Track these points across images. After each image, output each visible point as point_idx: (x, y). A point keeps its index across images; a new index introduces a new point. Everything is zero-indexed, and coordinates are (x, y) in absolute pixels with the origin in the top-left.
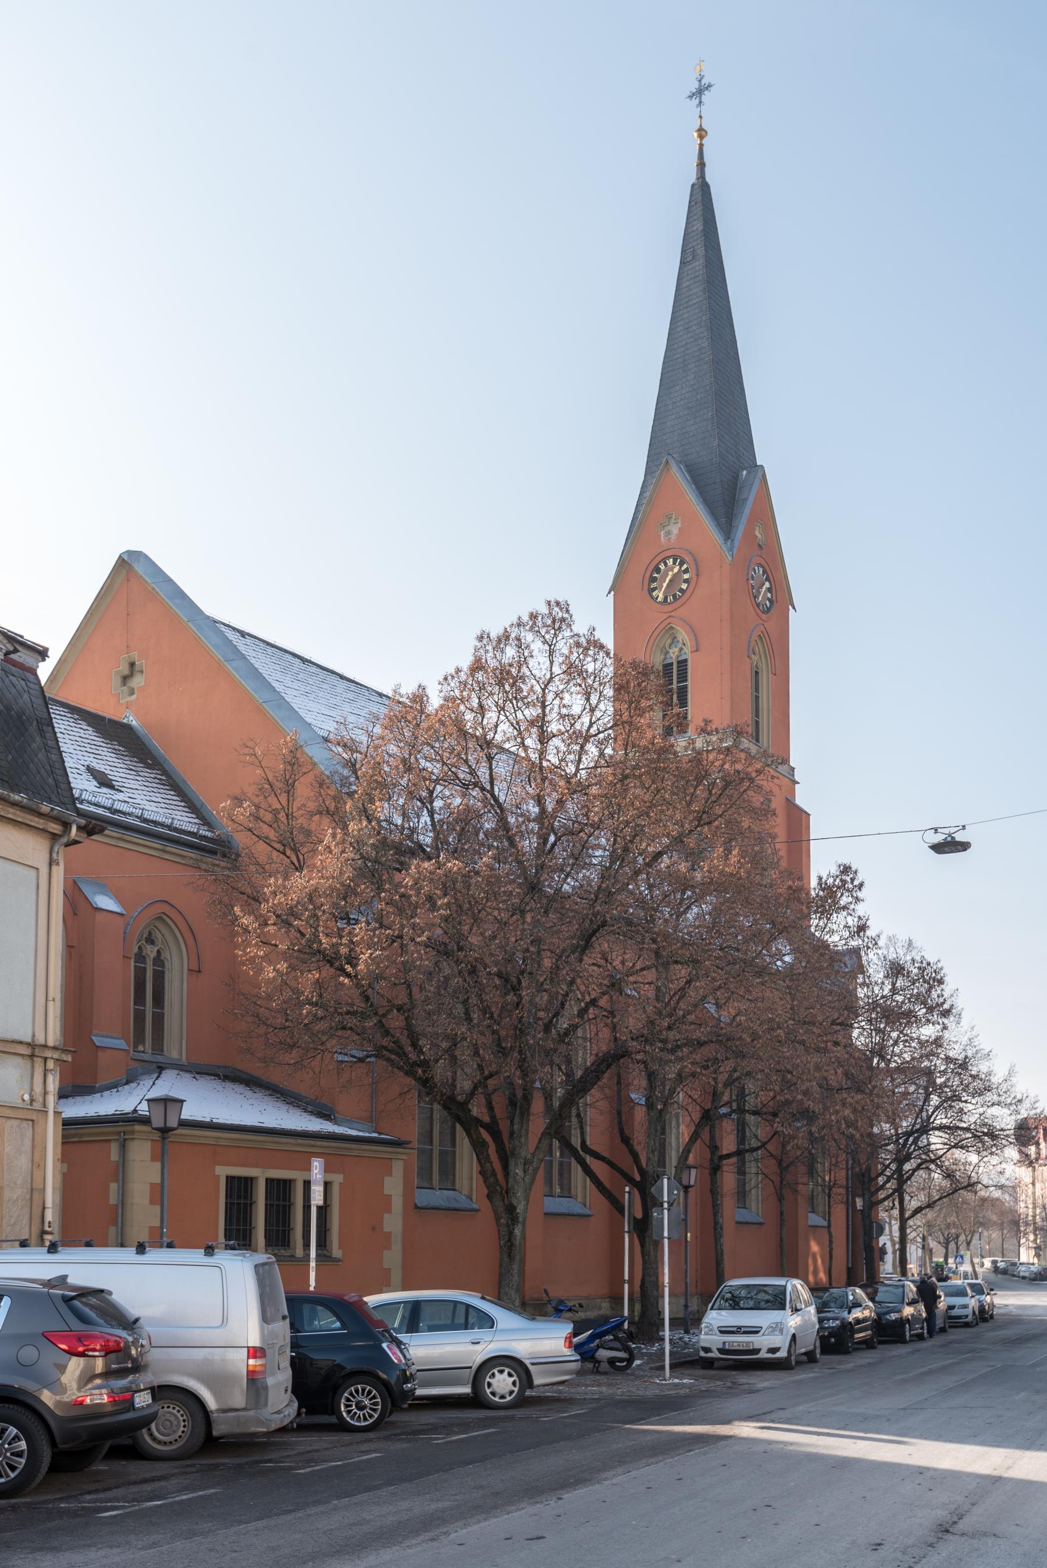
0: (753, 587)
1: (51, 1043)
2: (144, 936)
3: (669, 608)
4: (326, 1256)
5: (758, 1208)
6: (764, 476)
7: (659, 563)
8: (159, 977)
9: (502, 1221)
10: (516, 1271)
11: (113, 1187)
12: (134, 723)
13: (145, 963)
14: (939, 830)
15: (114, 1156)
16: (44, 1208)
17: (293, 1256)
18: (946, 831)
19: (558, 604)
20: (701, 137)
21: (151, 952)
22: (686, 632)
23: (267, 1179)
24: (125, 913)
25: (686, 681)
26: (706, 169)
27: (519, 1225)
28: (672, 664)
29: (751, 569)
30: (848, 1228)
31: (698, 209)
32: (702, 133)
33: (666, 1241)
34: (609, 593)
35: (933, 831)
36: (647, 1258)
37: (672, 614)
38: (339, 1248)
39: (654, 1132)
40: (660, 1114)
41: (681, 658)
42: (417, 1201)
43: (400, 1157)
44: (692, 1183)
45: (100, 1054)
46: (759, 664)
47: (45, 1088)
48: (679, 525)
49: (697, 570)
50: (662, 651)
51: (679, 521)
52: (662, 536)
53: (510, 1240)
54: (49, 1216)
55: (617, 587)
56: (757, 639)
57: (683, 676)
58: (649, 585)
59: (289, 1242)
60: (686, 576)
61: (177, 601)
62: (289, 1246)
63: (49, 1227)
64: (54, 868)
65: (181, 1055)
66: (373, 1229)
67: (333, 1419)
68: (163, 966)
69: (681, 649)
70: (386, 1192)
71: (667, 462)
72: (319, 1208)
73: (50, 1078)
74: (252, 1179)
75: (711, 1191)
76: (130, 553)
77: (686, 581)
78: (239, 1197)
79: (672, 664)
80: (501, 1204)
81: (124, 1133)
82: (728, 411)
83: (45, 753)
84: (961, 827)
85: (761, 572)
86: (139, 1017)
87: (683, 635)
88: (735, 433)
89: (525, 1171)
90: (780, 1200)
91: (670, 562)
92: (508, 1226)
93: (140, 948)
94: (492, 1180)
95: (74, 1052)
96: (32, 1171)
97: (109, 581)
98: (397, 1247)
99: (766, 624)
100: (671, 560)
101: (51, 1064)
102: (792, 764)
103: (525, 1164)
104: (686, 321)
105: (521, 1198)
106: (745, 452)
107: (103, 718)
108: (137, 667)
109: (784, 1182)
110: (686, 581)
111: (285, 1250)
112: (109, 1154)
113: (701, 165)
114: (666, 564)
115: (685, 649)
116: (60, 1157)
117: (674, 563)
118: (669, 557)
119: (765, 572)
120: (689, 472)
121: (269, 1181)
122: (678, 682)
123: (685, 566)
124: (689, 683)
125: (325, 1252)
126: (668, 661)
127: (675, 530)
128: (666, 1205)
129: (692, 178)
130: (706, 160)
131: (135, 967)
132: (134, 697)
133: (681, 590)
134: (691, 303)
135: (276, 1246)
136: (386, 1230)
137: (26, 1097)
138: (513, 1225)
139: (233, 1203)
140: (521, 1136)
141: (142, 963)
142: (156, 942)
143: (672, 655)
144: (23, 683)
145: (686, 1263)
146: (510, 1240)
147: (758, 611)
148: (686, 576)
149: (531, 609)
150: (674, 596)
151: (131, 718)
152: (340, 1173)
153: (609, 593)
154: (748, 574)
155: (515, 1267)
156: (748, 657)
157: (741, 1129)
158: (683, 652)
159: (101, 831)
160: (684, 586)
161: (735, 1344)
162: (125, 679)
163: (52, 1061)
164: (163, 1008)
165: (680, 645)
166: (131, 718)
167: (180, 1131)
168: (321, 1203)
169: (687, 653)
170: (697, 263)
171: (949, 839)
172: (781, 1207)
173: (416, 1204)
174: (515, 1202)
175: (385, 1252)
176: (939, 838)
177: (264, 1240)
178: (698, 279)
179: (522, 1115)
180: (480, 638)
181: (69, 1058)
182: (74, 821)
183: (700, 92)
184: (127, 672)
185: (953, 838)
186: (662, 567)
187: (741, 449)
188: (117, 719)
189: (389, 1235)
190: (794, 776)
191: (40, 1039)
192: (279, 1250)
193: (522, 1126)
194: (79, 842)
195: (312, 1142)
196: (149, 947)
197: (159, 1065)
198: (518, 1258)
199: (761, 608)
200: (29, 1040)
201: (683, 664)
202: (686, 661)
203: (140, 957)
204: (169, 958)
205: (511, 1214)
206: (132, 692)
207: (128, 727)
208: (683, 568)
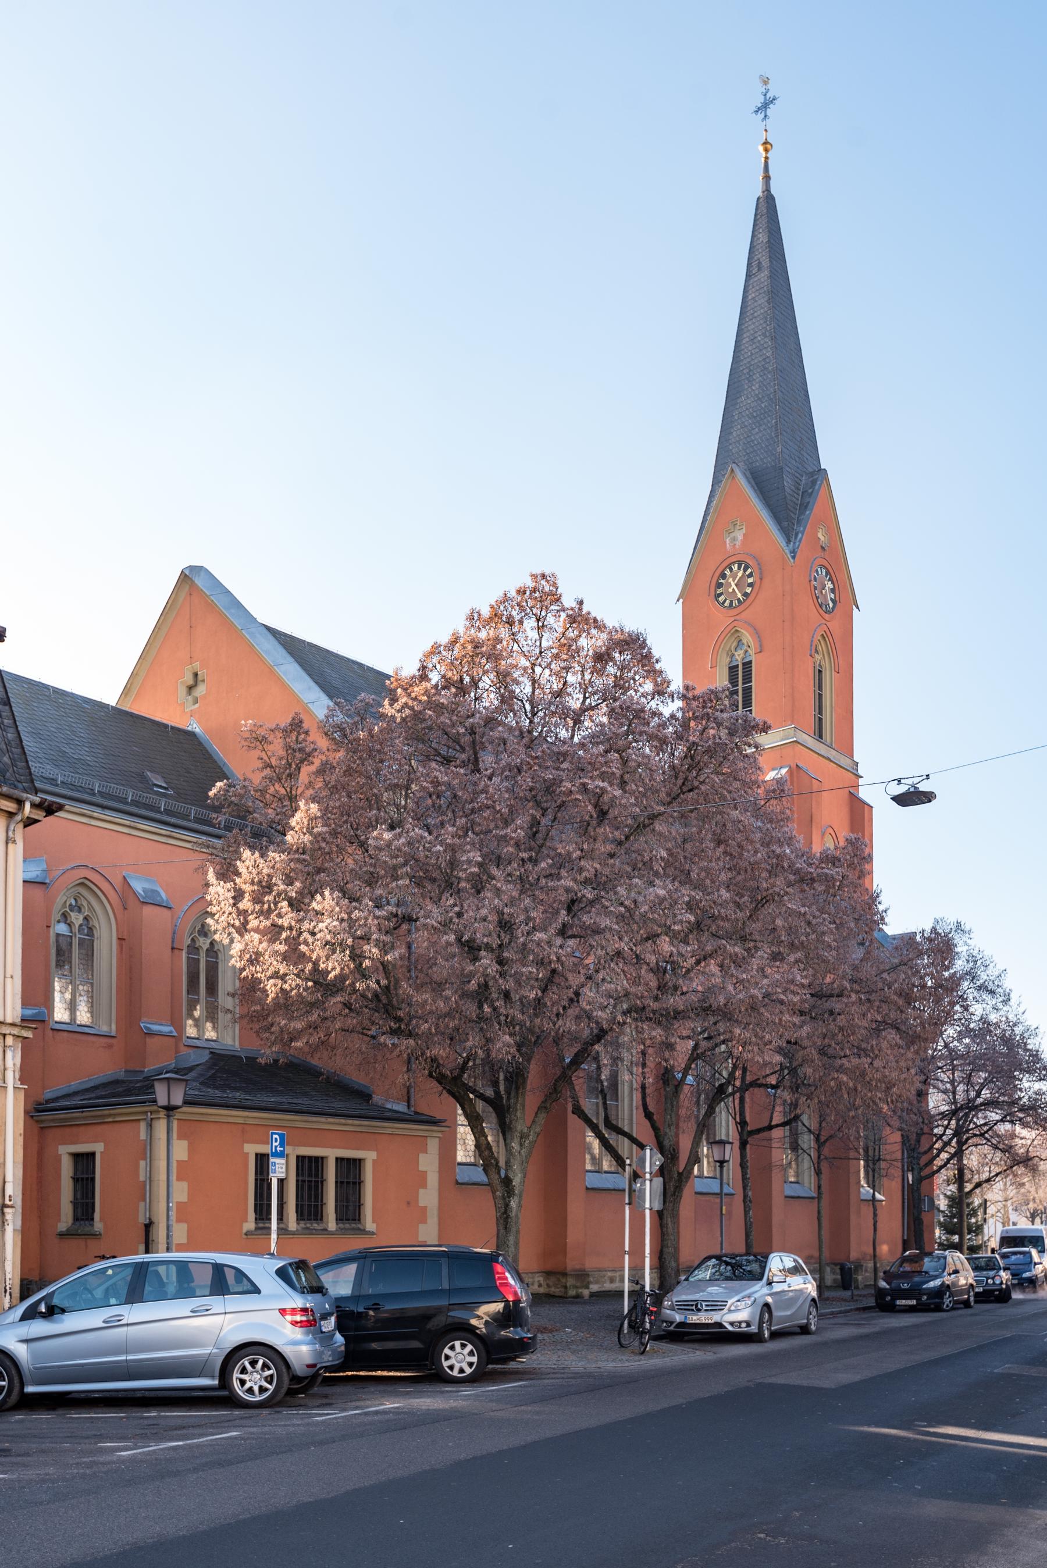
1: (9, 1020)
2: (197, 929)
3: (736, 611)
4: (359, 1229)
5: (810, 1183)
7: (725, 569)
9: (498, 1193)
10: (512, 1242)
11: (142, 1163)
12: (197, 730)
13: (199, 954)
14: (902, 781)
15: (143, 1135)
16: (4, 1182)
17: (326, 1230)
18: (910, 781)
19: (543, 576)
20: (766, 150)
22: (750, 635)
23: (298, 1157)
25: (751, 681)
26: (772, 182)
27: (515, 1197)
28: (737, 666)
29: (813, 570)
30: (903, 1202)
31: (763, 222)
34: (678, 600)
35: (896, 782)
36: (665, 1229)
37: (737, 618)
38: (373, 1222)
39: (670, 1107)
40: (676, 1089)
42: (458, 1178)
43: (435, 1134)
44: (727, 1158)
45: (148, 1040)
46: (823, 663)
47: (4, 1065)
48: (744, 531)
49: (761, 573)
50: (728, 654)
51: (744, 527)
52: (728, 542)
53: (505, 1212)
55: (687, 594)
56: (819, 638)
57: (748, 678)
58: (716, 591)
59: (322, 1216)
60: (750, 580)
61: (233, 611)
62: (321, 1219)
63: (10, 1200)
64: (10, 846)
65: (234, 1041)
66: (408, 1203)
68: (217, 957)
69: (746, 651)
70: (421, 1169)
71: (732, 470)
74: (322, 1158)
75: (741, 1165)
76: (191, 568)
77: (751, 585)
78: (310, 1175)
79: (737, 666)
80: (497, 1177)
81: (151, 1112)
82: (791, 417)
84: (925, 777)
85: (824, 574)
87: (747, 637)
88: (799, 439)
89: (521, 1145)
90: (817, 1174)
91: (735, 567)
92: (504, 1198)
93: (193, 940)
94: (486, 1153)
95: (35, 1028)
98: (433, 1220)
99: (828, 624)
100: (736, 565)
101: (10, 1040)
103: (521, 1138)
104: (752, 332)
105: (517, 1171)
107: (166, 726)
108: (200, 678)
109: (822, 1157)
110: (751, 585)
111: (318, 1224)
112: (139, 1133)
113: (767, 178)
114: (731, 570)
115: (750, 652)
116: (22, 1132)
117: (739, 568)
118: (734, 563)
119: (828, 573)
120: (754, 478)
121: (338, 1160)
122: (744, 683)
123: (749, 571)
124: (753, 684)
125: (359, 1226)
127: (739, 535)
128: (648, 1176)
129: (759, 192)
130: (771, 173)
131: (188, 958)
132: (197, 706)
134: (756, 314)
135: (308, 1220)
136: (421, 1203)
138: (509, 1197)
139: (304, 1181)
140: (516, 1110)
142: (83, 910)
143: (737, 657)
145: (722, 1236)
146: (505, 1212)
147: (821, 611)
148: (750, 580)
149: (519, 584)
151: (195, 726)
153: (678, 600)
154: (810, 575)
155: (512, 1238)
156: (811, 656)
157: (988, 1130)
158: (747, 654)
159: (61, 807)
160: (748, 590)
162: (190, 688)
163: (11, 1037)
165: (745, 648)
166: (195, 726)
167: (185, 1109)
169: (752, 657)
170: (762, 275)
171: (912, 790)
172: (819, 1180)
173: (457, 1181)
174: (511, 1175)
175: (420, 1225)
176: (902, 789)
177: (334, 1215)
178: (762, 291)
179: (517, 1089)
180: (471, 618)
181: (29, 1034)
182: (27, 799)
183: (765, 106)
184: (191, 682)
185: (915, 788)
186: (728, 572)
187: (805, 454)
188: (181, 727)
189: (425, 1208)
192: (312, 1224)
193: (517, 1101)
194: (36, 821)
195: (343, 1121)
196: (201, 939)
198: (514, 1230)
199: (824, 608)
201: (747, 665)
202: (750, 662)
203: (193, 948)
204: (222, 949)
205: (507, 1187)
206: (196, 701)
207: (192, 735)
208: (747, 573)
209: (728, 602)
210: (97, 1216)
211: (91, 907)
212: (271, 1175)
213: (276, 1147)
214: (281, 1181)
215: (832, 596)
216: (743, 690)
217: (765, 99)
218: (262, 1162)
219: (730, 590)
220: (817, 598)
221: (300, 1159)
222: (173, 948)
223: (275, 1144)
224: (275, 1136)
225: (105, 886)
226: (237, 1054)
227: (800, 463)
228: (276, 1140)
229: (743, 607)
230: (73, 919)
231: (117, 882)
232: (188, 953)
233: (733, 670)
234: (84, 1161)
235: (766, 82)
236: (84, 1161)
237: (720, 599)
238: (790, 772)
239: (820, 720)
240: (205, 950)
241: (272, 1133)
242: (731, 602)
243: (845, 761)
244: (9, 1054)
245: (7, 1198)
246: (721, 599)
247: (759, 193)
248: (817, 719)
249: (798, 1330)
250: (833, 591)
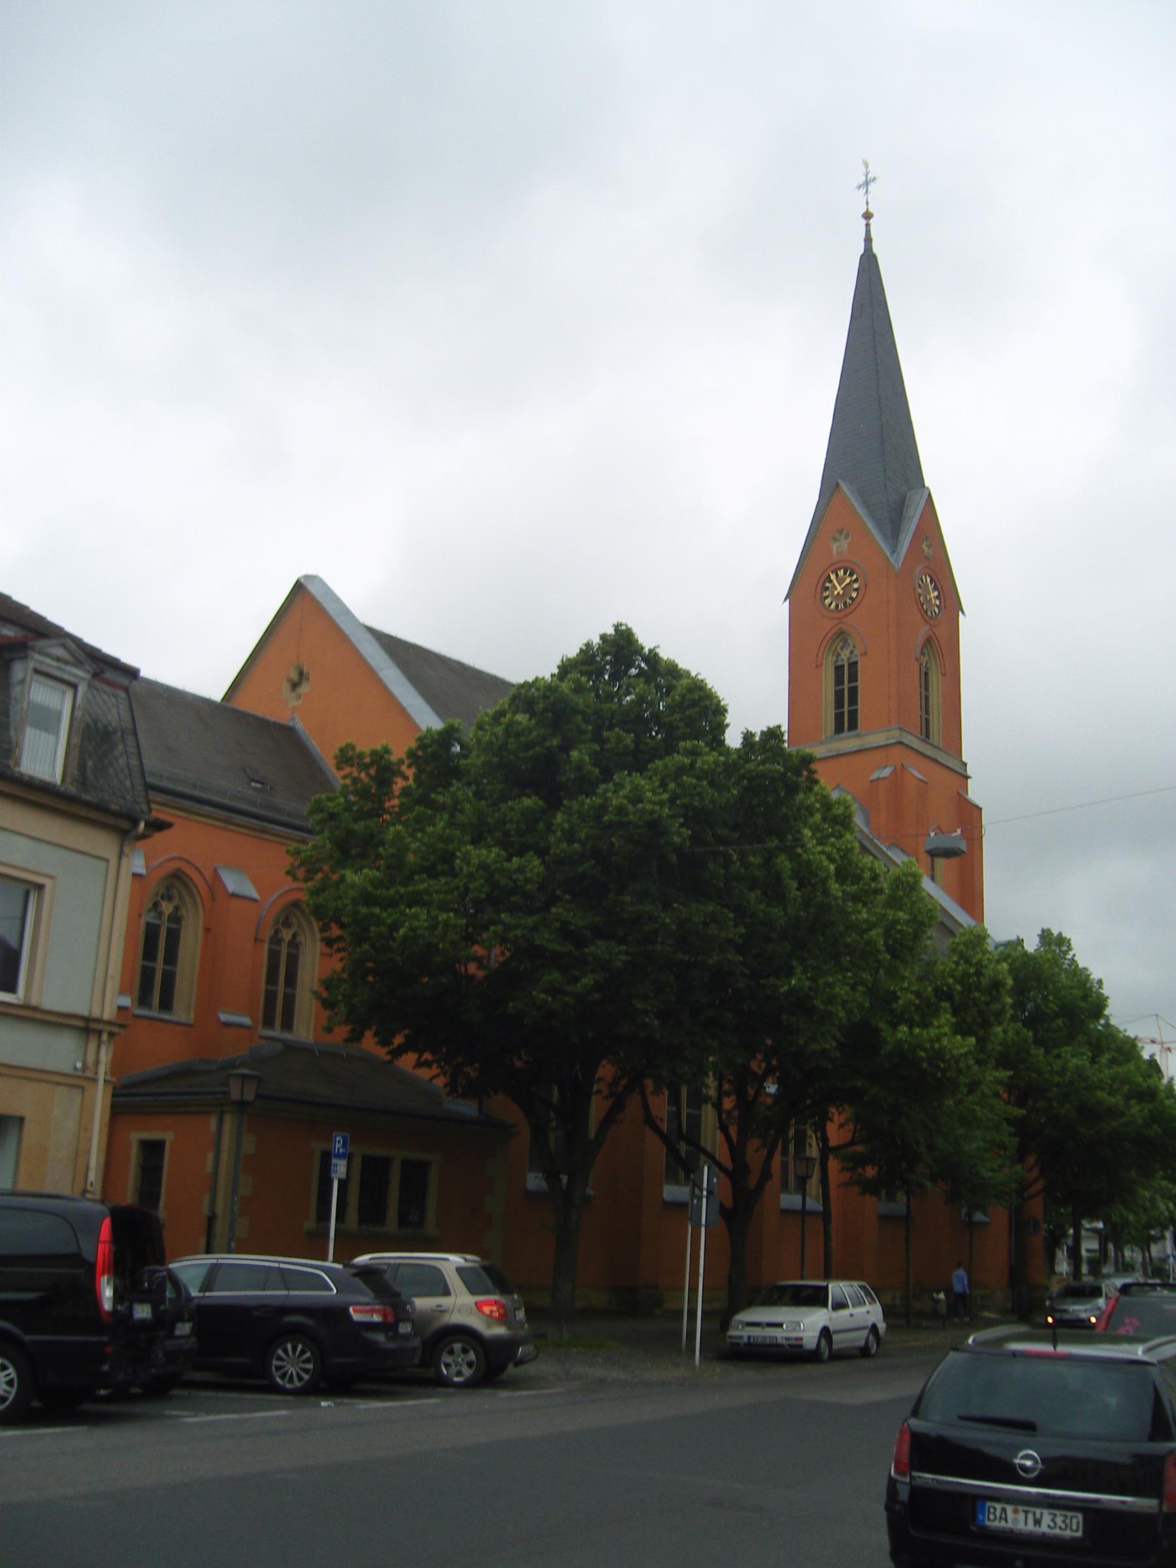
0: (920, 595)
1: (106, 1016)
3: (840, 615)
6: (930, 495)
8: (293, 961)
21: (287, 935)
25: (857, 681)
32: (868, 216)
41: (851, 661)
57: (853, 677)
60: (856, 586)
67: (266, 1382)
73: (103, 1049)
76: (307, 577)
79: (843, 666)
86: (270, 998)
97: (288, 600)
100: (842, 571)
102: (964, 759)
113: (868, 240)
115: (856, 652)
117: (845, 573)
121: (406, 1163)
123: (854, 577)
124: (859, 683)
126: (840, 663)
130: (873, 235)
133: (851, 598)
137: (79, 1065)
148: (856, 586)
150: (845, 604)
152: (779, 1197)
160: (854, 595)
162: (295, 686)
168: (343, 1176)
191: (96, 1013)
200: (86, 1013)
201: (853, 666)
202: (856, 663)
210: (162, 1204)
213: (338, 1149)
214: (342, 1183)
217: (867, 179)
219: (836, 593)
220: (922, 605)
221: (366, 1160)
225: (196, 877)
228: (339, 1142)
229: (849, 610)
233: (839, 669)
235: (866, 165)
236: (152, 1150)
239: (927, 721)
240: (287, 942)
246: (827, 601)
247: (862, 251)
248: (924, 720)
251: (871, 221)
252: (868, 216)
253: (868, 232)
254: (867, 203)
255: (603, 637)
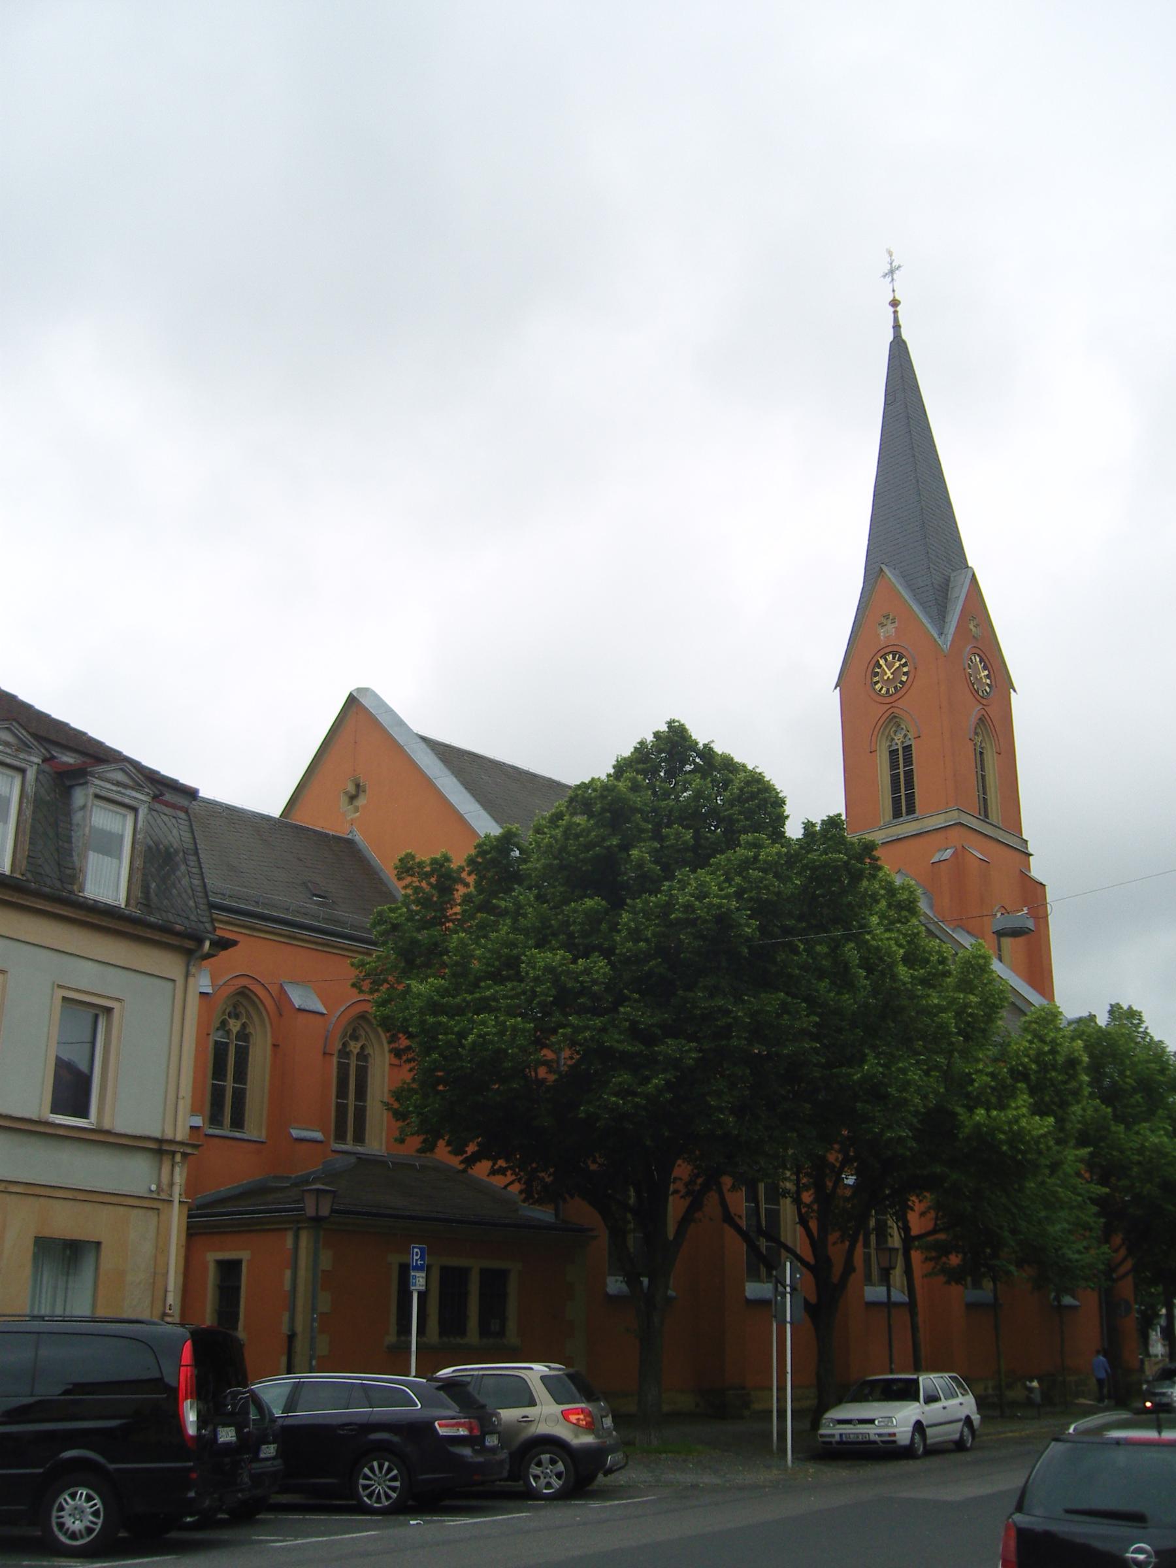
0: (970, 675)
1: (179, 1138)
6: (974, 575)
8: (362, 1073)
16: (166, 1291)
21: (355, 1047)
24: (325, 1012)
25: (912, 765)
32: (895, 303)
33: (788, 1326)
37: (893, 704)
54: (170, 1299)
55: (842, 682)
57: (908, 760)
60: (905, 669)
63: (170, 1309)
68: (366, 1061)
69: (905, 736)
72: (420, 1294)
76: (359, 690)
77: (905, 674)
83: (188, 880)
86: (341, 1110)
96: (156, 1256)
100: (891, 656)
106: (955, 556)
107: (327, 835)
110: (905, 674)
113: (897, 327)
117: (894, 658)
118: (888, 654)
122: (904, 767)
123: (904, 660)
130: (901, 322)
131: (339, 1063)
133: (902, 682)
141: (346, 1059)
143: (897, 741)
144: (174, 820)
148: (905, 669)
150: (895, 688)
158: (894, 743)
160: (904, 678)
161: (852, 1436)
162: (352, 798)
164: (365, 1101)
165: (904, 732)
190: (1027, 848)
191: (169, 1135)
196: (352, 1043)
197: (358, 1156)
201: (907, 749)
206: (357, 810)
209: (884, 689)
211: (249, 1016)
212: (412, 1288)
215: (988, 681)
216: (905, 773)
217: (891, 267)
218: (404, 1271)
220: (973, 684)
221: (444, 1270)
222: (325, 1054)
223: (415, 1258)
224: (416, 1250)
226: (384, 1159)
227: (948, 563)
230: (231, 1027)
231: (274, 990)
232: (340, 1057)
233: (893, 753)
234: (229, 1269)
235: (890, 254)
236: (229, 1269)
237: (877, 687)
238: (955, 854)
239: (985, 800)
241: (414, 1248)
242: (888, 690)
243: (1011, 841)
244: (177, 1170)
245: (168, 1308)
246: (878, 687)
247: (891, 338)
249: (952, 1446)
250: (988, 676)
251: (899, 309)
252: (895, 303)
253: (896, 319)
254: (894, 291)
255: (657, 735)
